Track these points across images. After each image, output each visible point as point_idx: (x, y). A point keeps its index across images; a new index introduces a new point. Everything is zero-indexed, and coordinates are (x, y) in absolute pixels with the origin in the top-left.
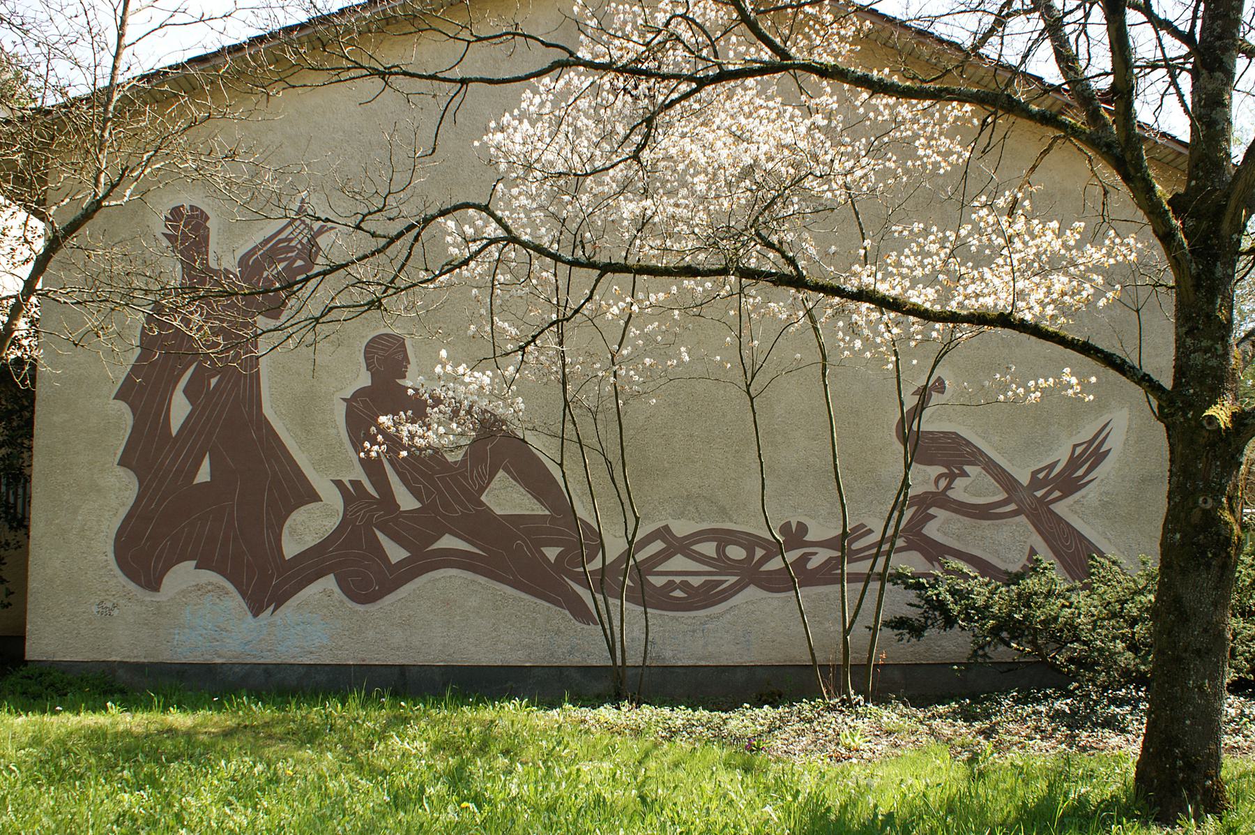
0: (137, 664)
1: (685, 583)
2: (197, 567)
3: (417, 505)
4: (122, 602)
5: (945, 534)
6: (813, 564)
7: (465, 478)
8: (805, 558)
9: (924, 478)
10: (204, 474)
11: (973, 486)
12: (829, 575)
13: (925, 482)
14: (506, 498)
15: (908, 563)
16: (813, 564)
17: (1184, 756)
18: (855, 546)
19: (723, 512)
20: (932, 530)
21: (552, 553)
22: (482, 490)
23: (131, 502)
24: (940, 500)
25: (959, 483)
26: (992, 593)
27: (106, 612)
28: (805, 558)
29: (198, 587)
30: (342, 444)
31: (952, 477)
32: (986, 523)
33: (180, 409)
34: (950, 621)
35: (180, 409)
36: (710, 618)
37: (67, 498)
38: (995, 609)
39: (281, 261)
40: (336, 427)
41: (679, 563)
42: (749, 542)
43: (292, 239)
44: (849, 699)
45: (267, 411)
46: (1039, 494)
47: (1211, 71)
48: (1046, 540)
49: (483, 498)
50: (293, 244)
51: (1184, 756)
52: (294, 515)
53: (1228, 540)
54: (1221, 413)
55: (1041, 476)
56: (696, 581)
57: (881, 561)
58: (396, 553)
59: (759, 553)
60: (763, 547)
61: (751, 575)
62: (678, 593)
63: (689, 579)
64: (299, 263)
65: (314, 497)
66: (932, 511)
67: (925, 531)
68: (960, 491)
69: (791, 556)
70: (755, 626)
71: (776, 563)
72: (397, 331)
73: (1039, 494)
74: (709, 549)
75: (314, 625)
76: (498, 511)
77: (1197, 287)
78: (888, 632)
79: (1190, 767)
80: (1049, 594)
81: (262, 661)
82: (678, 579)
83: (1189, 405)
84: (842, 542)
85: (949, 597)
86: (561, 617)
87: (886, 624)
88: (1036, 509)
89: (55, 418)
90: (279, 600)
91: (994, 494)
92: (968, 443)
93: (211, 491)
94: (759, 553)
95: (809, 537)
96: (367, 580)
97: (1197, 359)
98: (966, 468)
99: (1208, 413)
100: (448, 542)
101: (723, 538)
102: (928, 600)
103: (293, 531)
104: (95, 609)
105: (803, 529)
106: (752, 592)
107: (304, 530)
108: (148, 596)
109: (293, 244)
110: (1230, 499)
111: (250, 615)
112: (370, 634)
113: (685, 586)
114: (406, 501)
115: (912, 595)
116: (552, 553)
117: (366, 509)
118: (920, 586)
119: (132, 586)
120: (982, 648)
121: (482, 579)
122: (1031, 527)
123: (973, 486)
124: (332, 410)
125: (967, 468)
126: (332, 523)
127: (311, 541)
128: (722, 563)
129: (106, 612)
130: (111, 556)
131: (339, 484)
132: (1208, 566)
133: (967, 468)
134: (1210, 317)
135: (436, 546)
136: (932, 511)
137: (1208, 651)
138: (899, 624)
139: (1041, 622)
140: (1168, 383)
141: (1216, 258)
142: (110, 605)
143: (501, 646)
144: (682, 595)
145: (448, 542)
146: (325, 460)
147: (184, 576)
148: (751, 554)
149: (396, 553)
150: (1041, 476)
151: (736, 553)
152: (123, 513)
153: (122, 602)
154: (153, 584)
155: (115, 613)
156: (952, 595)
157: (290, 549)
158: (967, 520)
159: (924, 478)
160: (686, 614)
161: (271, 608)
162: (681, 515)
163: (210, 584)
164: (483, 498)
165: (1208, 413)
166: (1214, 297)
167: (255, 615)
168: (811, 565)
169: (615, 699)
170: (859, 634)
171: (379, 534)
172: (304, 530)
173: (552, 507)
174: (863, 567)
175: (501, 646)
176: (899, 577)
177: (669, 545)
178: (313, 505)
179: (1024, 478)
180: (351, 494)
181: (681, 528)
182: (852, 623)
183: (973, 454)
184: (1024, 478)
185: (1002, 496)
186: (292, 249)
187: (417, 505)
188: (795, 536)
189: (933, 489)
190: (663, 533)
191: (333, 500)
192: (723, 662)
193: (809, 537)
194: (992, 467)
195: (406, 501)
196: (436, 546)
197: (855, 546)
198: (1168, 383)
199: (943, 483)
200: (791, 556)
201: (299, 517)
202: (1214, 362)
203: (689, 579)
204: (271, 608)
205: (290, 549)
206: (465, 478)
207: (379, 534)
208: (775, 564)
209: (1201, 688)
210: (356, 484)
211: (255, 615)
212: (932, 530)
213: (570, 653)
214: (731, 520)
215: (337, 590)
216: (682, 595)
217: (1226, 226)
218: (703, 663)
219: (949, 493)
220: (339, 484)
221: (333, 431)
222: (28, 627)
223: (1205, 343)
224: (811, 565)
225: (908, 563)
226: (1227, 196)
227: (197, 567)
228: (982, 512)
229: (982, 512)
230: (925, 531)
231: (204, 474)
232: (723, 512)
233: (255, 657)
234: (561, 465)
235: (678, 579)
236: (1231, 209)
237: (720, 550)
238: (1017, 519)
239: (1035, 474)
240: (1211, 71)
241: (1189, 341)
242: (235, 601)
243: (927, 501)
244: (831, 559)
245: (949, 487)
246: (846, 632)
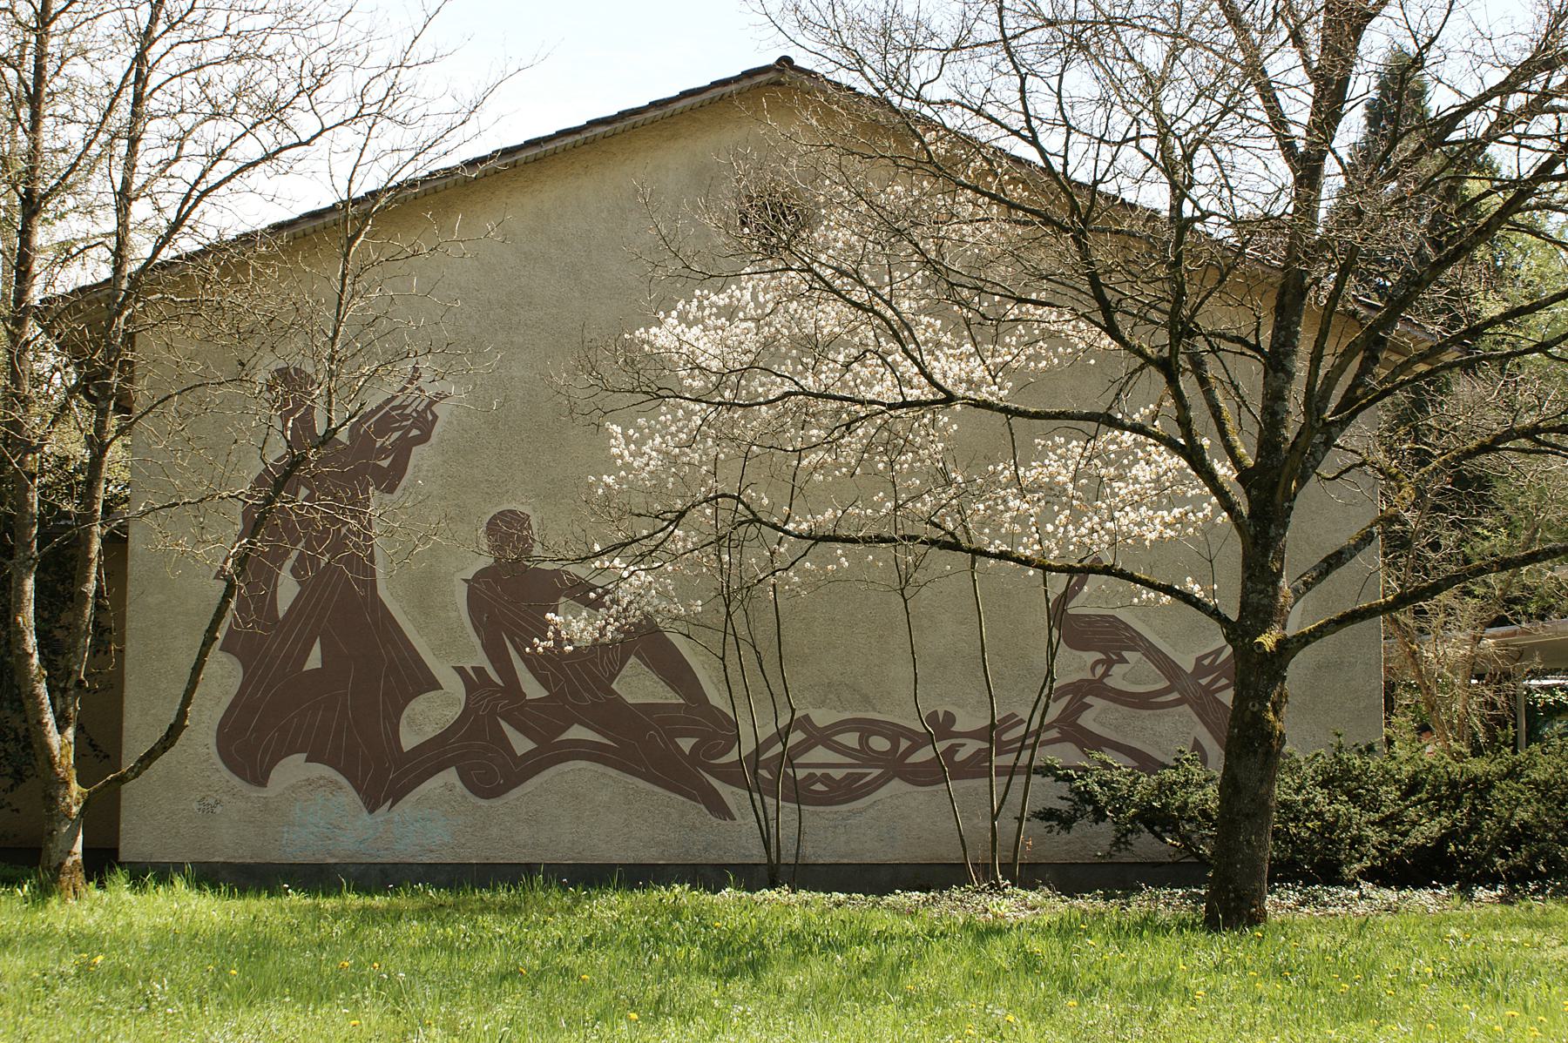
0: (243, 865)
1: (826, 776)
2: (307, 760)
3: (545, 693)
4: (225, 798)
5: (1103, 724)
6: (961, 756)
7: (596, 665)
8: (952, 750)
9: (1075, 665)
10: (314, 660)
11: (1132, 673)
12: (976, 767)
13: (1082, 669)
14: (638, 686)
15: (1058, 755)
16: (961, 756)
17: (1235, 890)
18: (1005, 737)
19: (866, 700)
20: (1087, 720)
21: (686, 744)
22: (613, 677)
23: (235, 690)
24: (1097, 688)
25: (1117, 669)
26: (1134, 783)
27: (208, 809)
28: (952, 750)
29: (309, 782)
30: (463, 628)
31: (1109, 664)
32: (1146, 713)
33: (287, 590)
34: (1099, 815)
35: (287, 590)
36: (853, 813)
37: (163, 686)
38: (1136, 798)
39: (397, 429)
40: (457, 610)
41: (819, 754)
42: (895, 733)
43: (406, 407)
44: (998, 884)
45: (383, 592)
46: (1204, 682)
47: (1276, 371)
48: (1211, 731)
49: (614, 686)
50: (408, 411)
51: (1235, 890)
52: (413, 704)
53: (1270, 735)
54: (1268, 641)
55: (1206, 662)
56: (838, 774)
57: (1026, 755)
58: (522, 745)
59: (904, 744)
60: (908, 738)
61: (896, 767)
62: (819, 787)
63: (831, 772)
64: (415, 432)
65: (434, 685)
66: (1088, 700)
67: (1080, 721)
68: (1118, 678)
69: (941, 746)
70: (903, 817)
71: (919, 755)
72: (520, 508)
73: (1204, 682)
74: (851, 739)
75: (434, 820)
76: (630, 700)
77: (1255, 544)
78: (1039, 826)
79: (1239, 898)
80: (1187, 783)
81: (379, 860)
82: (819, 772)
83: (1246, 633)
84: (991, 732)
85: (1097, 788)
86: (696, 812)
87: (1036, 815)
88: (1200, 698)
89: (149, 599)
90: (397, 795)
91: (1156, 682)
92: (1127, 627)
93: (321, 683)
94: (904, 744)
95: (957, 728)
96: (491, 773)
97: (1254, 598)
98: (1125, 654)
99: (1259, 640)
100: (577, 732)
101: (866, 728)
102: (1076, 791)
103: (411, 722)
104: (195, 806)
105: (950, 718)
106: (896, 785)
107: (425, 720)
108: (255, 793)
109: (408, 411)
110: (1273, 704)
111: (365, 812)
112: (495, 831)
113: (826, 779)
114: (533, 689)
115: (1064, 789)
116: (686, 744)
117: (489, 699)
118: (1069, 779)
119: (236, 781)
120: (1125, 835)
121: (613, 772)
122: (1196, 719)
123: (1132, 673)
124: (453, 592)
125: (1126, 654)
126: (454, 712)
127: (431, 731)
128: (866, 755)
129: (208, 809)
130: (214, 749)
131: (460, 671)
132: (1255, 752)
133: (1126, 654)
134: (1264, 567)
135: (564, 737)
136: (1088, 700)
137: (1255, 815)
138: (1048, 815)
139: (1178, 809)
140: (1234, 617)
141: (1271, 521)
142: (212, 801)
143: (633, 843)
144: (823, 788)
145: (577, 732)
146: (447, 645)
147: (293, 770)
148: (895, 745)
149: (522, 745)
150: (1206, 662)
151: (880, 744)
152: (226, 701)
153: (225, 798)
154: (260, 780)
155: (218, 810)
156: (1101, 786)
157: (409, 741)
158: (1125, 710)
159: (1075, 665)
160: (828, 809)
161: (388, 804)
162: (821, 704)
163: (321, 778)
164: (614, 686)
165: (1259, 640)
166: (1268, 551)
167: (371, 811)
168: (959, 757)
169: (772, 885)
170: (1007, 825)
171: (504, 725)
172: (425, 720)
173: (687, 697)
174: (1008, 760)
175: (633, 843)
176: (1048, 770)
177: (810, 736)
178: (432, 693)
179: (1188, 665)
180: (474, 682)
181: (823, 717)
182: (999, 809)
183: (1132, 639)
184: (1188, 665)
185: (1165, 684)
186: (406, 417)
187: (545, 693)
188: (942, 726)
189: (1090, 677)
190: (805, 723)
191: (454, 687)
192: (867, 859)
193: (957, 728)
194: (1152, 653)
195: (533, 689)
196: (564, 737)
197: (1005, 737)
198: (1234, 617)
199: (1100, 670)
200: (941, 746)
201: (418, 706)
202: (1265, 601)
203: (831, 772)
204: (388, 804)
205: (409, 741)
206: (596, 665)
207: (504, 725)
208: (924, 755)
209: (1249, 842)
210: (479, 671)
211: (371, 811)
212: (1087, 720)
213: (706, 850)
214: (874, 709)
215: (459, 783)
216: (823, 788)
217: (1279, 497)
218: (845, 861)
219: (1108, 681)
220: (460, 671)
221: (453, 614)
222: (122, 826)
223: (1260, 587)
224: (959, 757)
225: (1058, 755)
226: (1279, 476)
227: (307, 760)
228: (1142, 702)
229: (1142, 702)
230: (1080, 721)
231: (314, 660)
232: (866, 700)
233: (371, 855)
234: (722, 659)
235: (819, 772)
236: (1283, 481)
237: (863, 741)
238: (1180, 708)
239: (1199, 660)
240: (1276, 371)
241: (1249, 584)
242: (349, 797)
243: (1080, 691)
244: (980, 750)
245: (1106, 674)
246: (994, 817)
